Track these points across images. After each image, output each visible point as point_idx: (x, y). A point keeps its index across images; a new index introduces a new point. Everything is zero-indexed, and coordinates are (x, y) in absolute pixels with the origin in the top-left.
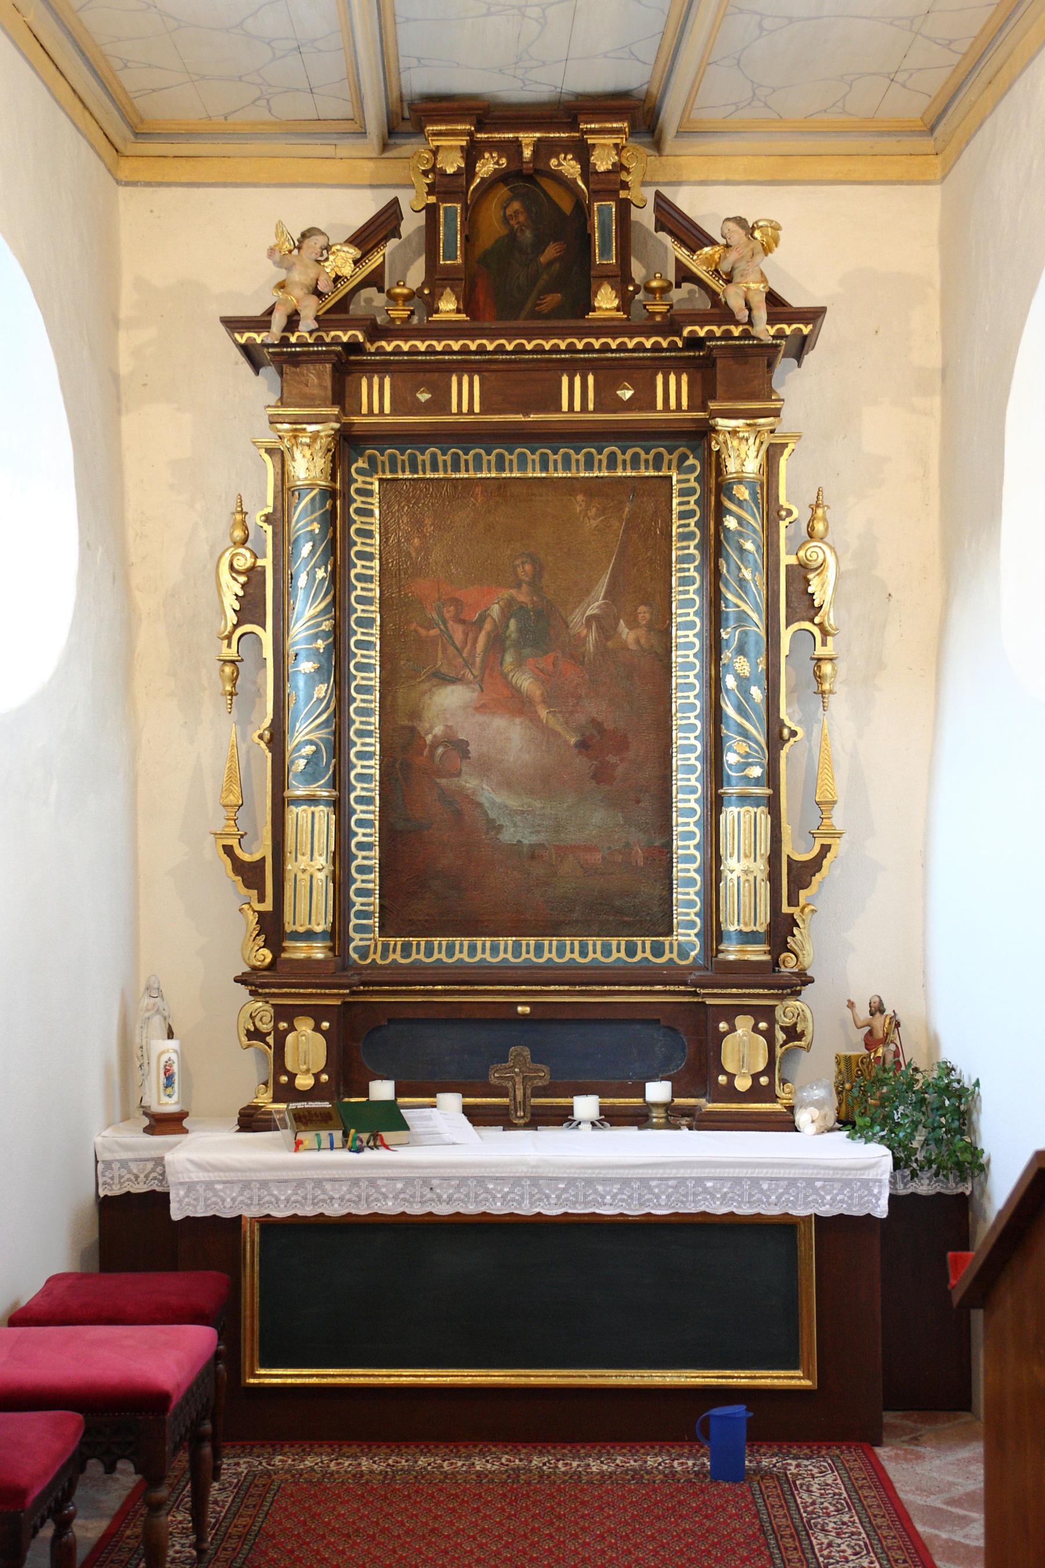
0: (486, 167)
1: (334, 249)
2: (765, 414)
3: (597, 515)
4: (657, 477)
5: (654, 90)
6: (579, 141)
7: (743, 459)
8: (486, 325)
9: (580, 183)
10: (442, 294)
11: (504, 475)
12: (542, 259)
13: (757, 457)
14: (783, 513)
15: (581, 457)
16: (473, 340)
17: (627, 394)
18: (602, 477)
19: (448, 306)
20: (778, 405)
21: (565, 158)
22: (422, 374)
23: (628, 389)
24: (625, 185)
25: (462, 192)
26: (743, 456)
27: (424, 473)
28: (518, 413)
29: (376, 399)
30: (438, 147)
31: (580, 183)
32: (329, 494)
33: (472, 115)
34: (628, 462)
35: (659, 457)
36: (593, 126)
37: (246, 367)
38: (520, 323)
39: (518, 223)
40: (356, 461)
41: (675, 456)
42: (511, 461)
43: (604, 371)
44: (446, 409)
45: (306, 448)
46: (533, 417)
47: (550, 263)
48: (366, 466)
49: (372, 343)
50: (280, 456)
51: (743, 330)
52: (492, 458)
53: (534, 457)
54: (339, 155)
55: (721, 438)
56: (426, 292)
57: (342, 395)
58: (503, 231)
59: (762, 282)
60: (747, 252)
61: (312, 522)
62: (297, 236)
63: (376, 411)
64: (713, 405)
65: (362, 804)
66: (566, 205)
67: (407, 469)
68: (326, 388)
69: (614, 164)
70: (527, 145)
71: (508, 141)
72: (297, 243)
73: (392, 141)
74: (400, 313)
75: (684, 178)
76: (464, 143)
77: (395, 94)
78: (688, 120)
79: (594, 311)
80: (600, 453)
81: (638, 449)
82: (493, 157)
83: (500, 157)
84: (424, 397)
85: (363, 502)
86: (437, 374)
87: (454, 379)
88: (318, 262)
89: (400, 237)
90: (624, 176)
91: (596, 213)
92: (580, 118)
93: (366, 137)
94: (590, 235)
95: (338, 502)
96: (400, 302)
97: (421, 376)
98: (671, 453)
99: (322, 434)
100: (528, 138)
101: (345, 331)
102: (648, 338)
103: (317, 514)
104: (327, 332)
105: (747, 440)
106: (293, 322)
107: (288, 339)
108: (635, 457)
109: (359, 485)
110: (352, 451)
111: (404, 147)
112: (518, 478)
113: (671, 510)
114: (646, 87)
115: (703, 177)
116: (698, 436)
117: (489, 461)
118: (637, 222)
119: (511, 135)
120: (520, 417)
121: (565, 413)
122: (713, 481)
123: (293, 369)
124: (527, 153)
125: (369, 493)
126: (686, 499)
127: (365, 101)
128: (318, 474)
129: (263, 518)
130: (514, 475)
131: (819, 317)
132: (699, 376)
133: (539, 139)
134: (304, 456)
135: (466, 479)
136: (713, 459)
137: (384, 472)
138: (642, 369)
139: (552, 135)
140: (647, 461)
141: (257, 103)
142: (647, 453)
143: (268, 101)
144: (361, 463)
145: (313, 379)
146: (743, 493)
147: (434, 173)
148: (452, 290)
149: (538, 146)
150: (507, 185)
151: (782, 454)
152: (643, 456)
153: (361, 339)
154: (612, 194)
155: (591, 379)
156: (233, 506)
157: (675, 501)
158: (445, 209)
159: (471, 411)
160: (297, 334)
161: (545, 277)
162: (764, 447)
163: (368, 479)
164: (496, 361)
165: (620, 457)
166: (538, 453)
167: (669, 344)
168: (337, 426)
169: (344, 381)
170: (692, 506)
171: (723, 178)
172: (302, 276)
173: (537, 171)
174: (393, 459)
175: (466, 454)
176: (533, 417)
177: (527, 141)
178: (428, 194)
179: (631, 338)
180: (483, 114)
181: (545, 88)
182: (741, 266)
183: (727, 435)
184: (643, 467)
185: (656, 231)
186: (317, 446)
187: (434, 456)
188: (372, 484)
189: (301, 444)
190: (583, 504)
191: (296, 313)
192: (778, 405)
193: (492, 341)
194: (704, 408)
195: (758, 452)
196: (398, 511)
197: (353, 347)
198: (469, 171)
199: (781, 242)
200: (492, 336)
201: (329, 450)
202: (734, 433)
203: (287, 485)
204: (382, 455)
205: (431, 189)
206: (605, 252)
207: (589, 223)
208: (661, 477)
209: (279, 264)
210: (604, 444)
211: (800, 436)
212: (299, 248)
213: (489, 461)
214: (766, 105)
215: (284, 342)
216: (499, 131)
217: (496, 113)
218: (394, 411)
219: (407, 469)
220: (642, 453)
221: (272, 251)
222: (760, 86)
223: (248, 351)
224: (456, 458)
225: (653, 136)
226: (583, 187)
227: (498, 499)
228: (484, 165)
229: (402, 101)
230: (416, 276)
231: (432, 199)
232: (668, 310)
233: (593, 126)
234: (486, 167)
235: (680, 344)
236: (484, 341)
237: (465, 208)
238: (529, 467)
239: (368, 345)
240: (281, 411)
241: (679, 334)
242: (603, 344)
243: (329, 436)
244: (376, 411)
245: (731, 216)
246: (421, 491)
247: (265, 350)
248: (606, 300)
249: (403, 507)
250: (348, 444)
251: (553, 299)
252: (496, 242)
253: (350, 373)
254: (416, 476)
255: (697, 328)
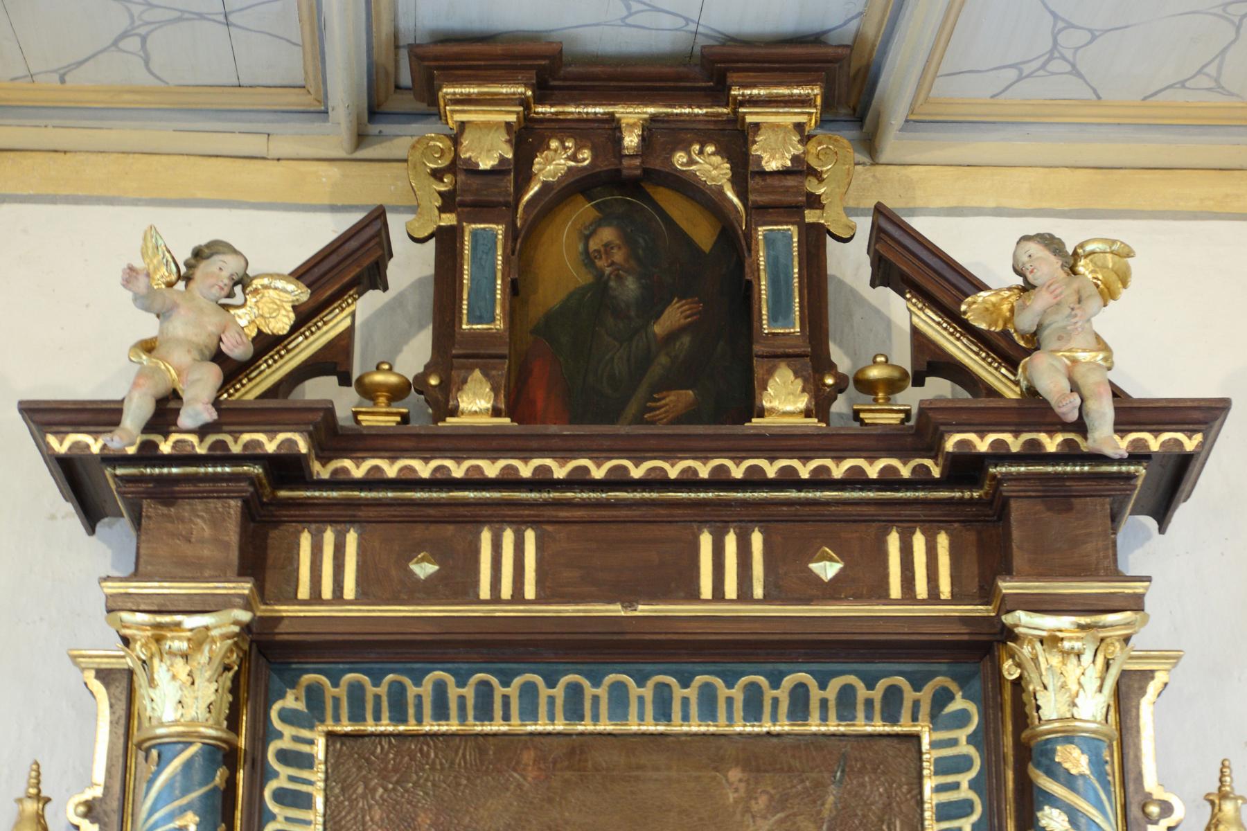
0: (553, 164)
1: (257, 283)
2: (1116, 605)
3: (772, 809)
4: (889, 735)
5: (870, 31)
6: (729, 121)
7: (1068, 689)
8: (553, 429)
9: (730, 194)
10: (465, 381)
11: (580, 728)
12: (659, 328)
13: (1100, 689)
14: (1154, 810)
15: (737, 693)
16: (526, 460)
17: (828, 570)
18: (778, 735)
19: (476, 403)
20: (1138, 587)
21: (701, 152)
22: (421, 527)
23: (831, 560)
24: (814, 202)
25: (507, 204)
26: (1074, 687)
27: (420, 721)
28: (611, 601)
29: (328, 574)
30: (462, 125)
31: (730, 194)
32: (223, 755)
33: (531, 67)
34: (832, 704)
35: (893, 695)
36: (755, 92)
37: (67, 510)
38: (622, 429)
39: (613, 264)
40: (282, 696)
41: (926, 695)
42: (596, 699)
43: (781, 526)
44: (467, 592)
45: (179, 662)
46: (643, 610)
47: (672, 336)
48: (301, 706)
49: (325, 461)
50: (123, 684)
51: (1066, 442)
52: (559, 692)
53: (641, 691)
54: (274, 153)
55: (1026, 650)
56: (434, 381)
57: (260, 560)
58: (583, 278)
59: (1099, 350)
60: (1069, 295)
61: (182, 811)
62: (183, 255)
63: (327, 593)
64: (1007, 586)
65: (477, 696)
66: (703, 234)
67: (385, 714)
68: (226, 545)
69: (795, 159)
70: (632, 126)
71: (596, 120)
72: (183, 270)
73: (374, 129)
74: (381, 419)
75: (919, 203)
76: (512, 118)
77: (385, 30)
78: (926, 100)
79: (761, 415)
80: (775, 684)
81: (852, 679)
82: (565, 148)
83: (579, 148)
84: (424, 569)
85: (292, 779)
86: (451, 528)
87: (486, 537)
88: (226, 307)
89: (385, 288)
90: (812, 186)
91: (761, 244)
92: (732, 77)
93: (326, 120)
94: (749, 283)
95: (241, 775)
96: (382, 400)
97: (419, 531)
98: (917, 687)
99: (215, 633)
100: (632, 117)
101: (272, 433)
102: (871, 459)
103: (195, 795)
104: (235, 435)
105: (1079, 656)
106: (165, 412)
107: (156, 446)
108: (847, 694)
109: (285, 743)
110: (275, 677)
111: (397, 141)
112: (610, 734)
113: (921, 802)
114: (853, 25)
115: (952, 202)
116: (976, 654)
117: (551, 700)
118: (834, 277)
119: (599, 110)
120: (615, 610)
121: (706, 601)
122: (1008, 741)
123: (164, 510)
124: (631, 140)
125: (305, 761)
126: (950, 779)
127: (328, 35)
128: (202, 713)
129: (82, 809)
130: (600, 728)
131: (1216, 419)
132: (971, 536)
133: (654, 119)
134: (174, 677)
135: (505, 734)
136: (1008, 695)
137: (337, 719)
138: (858, 524)
139: (677, 111)
140: (869, 703)
141: (121, 45)
142: (870, 686)
143: (144, 39)
144: (292, 701)
145: (202, 528)
146: (1075, 760)
147: (455, 174)
148: (486, 374)
149: (651, 128)
150: (590, 199)
151: (1142, 691)
152: (862, 692)
153: (303, 447)
154: (792, 211)
155: (757, 539)
156: (21, 786)
157: (929, 784)
158: (474, 234)
159: (518, 596)
160: (174, 437)
161: (663, 360)
162: (1114, 673)
163: (305, 733)
164: (569, 504)
165: (816, 694)
166: (651, 683)
167: (914, 470)
168: (245, 616)
169: (265, 538)
170: (965, 793)
171: (991, 204)
172: (191, 326)
173: (648, 174)
174: (357, 694)
175: (506, 684)
176: (643, 610)
177: (632, 119)
178: (442, 210)
179: (839, 459)
180: (548, 69)
181: (667, 21)
182: (1057, 321)
183: (1038, 646)
184: (861, 714)
185: (873, 284)
186: (203, 658)
187: (440, 688)
188: (311, 742)
189: (172, 654)
190: (742, 786)
191: (175, 395)
192: (1138, 587)
193: (563, 460)
194: (986, 593)
195: (1103, 680)
196: (364, 796)
197: (286, 468)
198: (521, 168)
199: (1133, 282)
200: (563, 451)
201: (227, 668)
202: (1052, 641)
203: (136, 736)
204: (336, 684)
205: (448, 202)
206: (780, 311)
207: (748, 262)
208: (897, 736)
209: (146, 301)
210: (783, 667)
211: (1178, 658)
212: (188, 279)
213: (551, 700)
214: (1075, 71)
215: (148, 454)
216: (577, 101)
217: (573, 69)
218: (364, 595)
219: (385, 714)
220: (860, 685)
221: (131, 274)
222: (1070, 26)
223: (73, 475)
224: (485, 692)
225: (861, 127)
226: (736, 200)
227: (568, 774)
228: (548, 161)
229: (397, 47)
230: (414, 356)
231: (449, 219)
232: (903, 421)
233: (755, 92)
234: (553, 164)
235: (936, 472)
236: (548, 462)
237: (513, 234)
238: (628, 709)
239: (316, 467)
240: (135, 588)
241: (933, 450)
242: (783, 470)
243: (226, 637)
244: (327, 593)
245: (1032, 233)
246: (412, 758)
247: (108, 471)
248: (784, 399)
249: (374, 790)
250: (264, 661)
251: (679, 399)
252: (571, 295)
253: (277, 523)
254: (402, 728)
255: (972, 437)
